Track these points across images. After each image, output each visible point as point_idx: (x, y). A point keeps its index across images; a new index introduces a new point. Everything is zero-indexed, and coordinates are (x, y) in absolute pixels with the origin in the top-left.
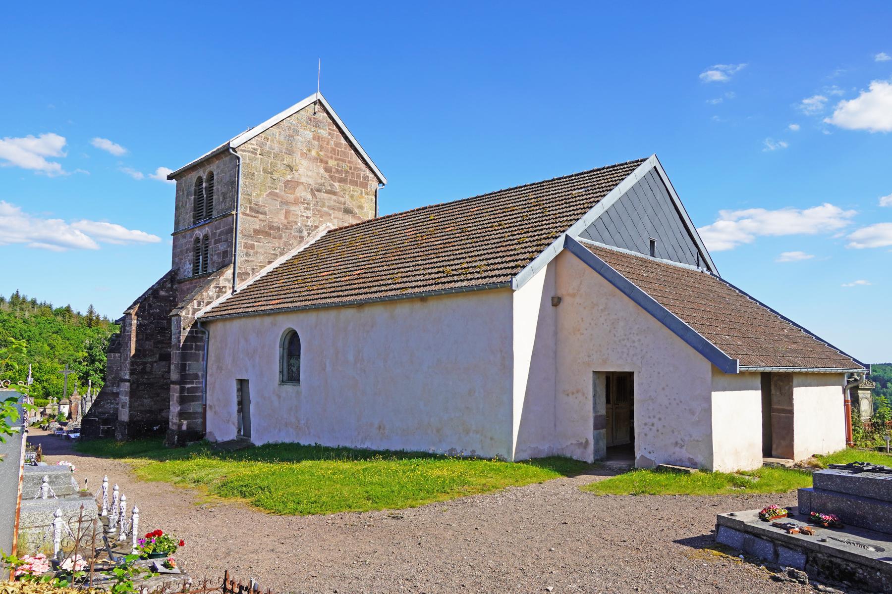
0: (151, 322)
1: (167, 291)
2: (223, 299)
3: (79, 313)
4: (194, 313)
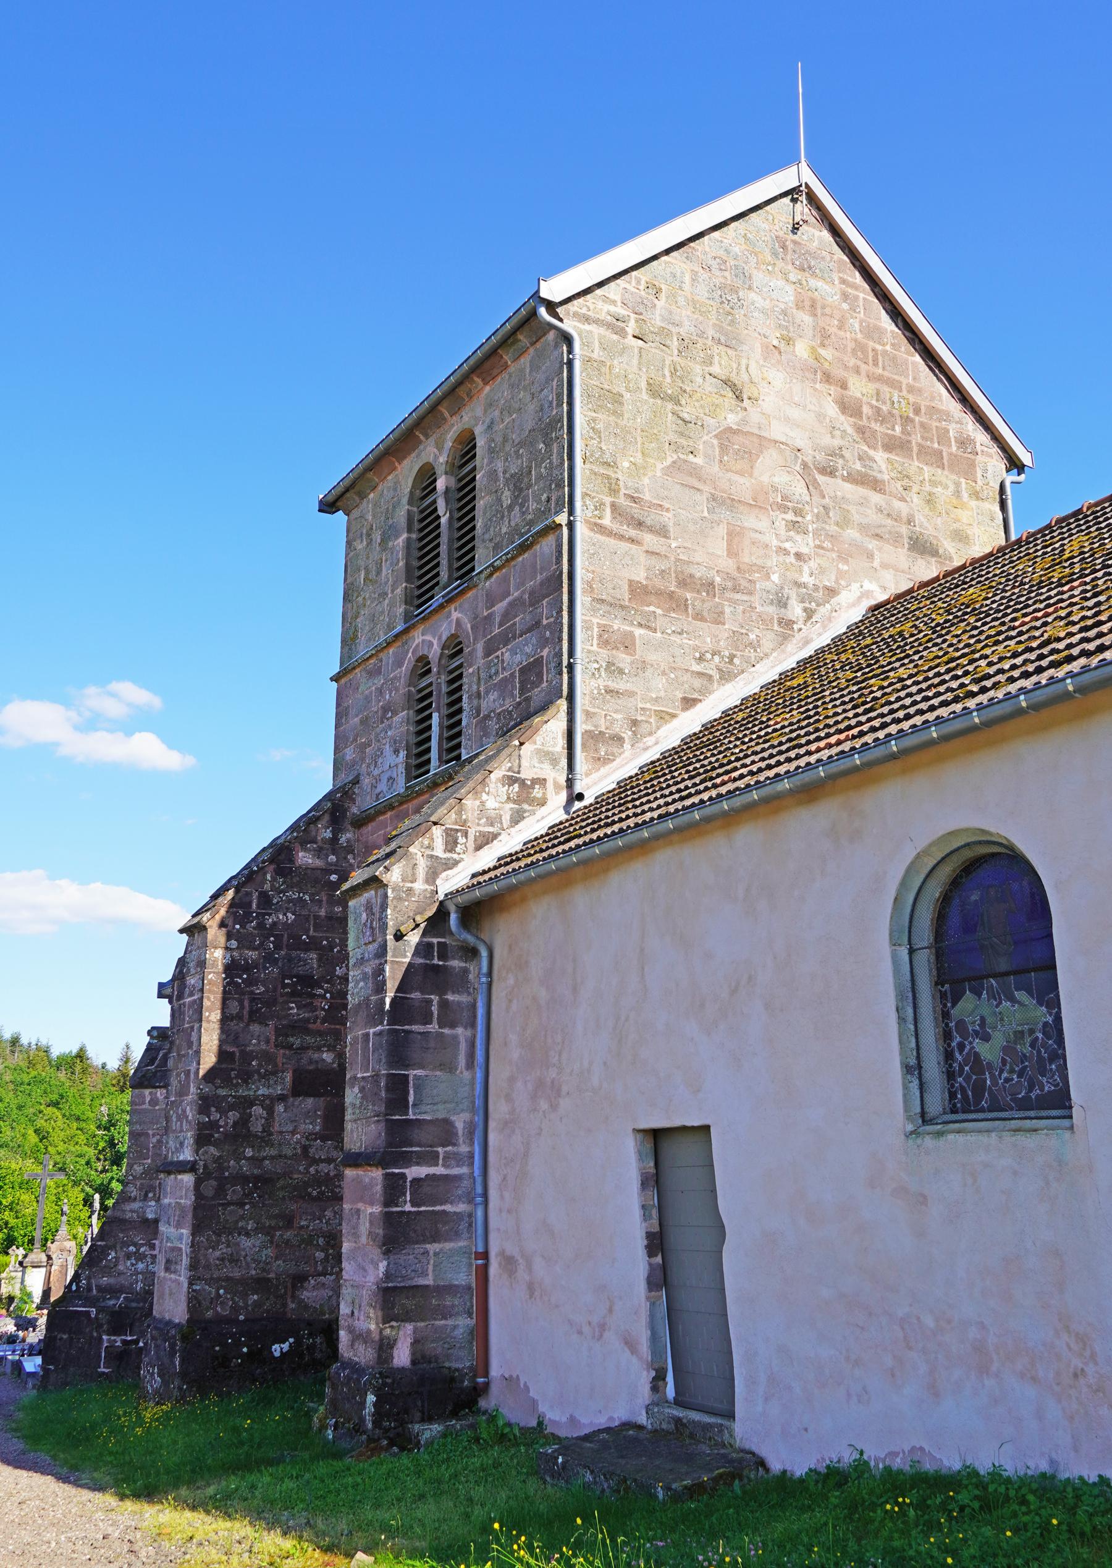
0: (269, 958)
1: (319, 853)
2: (536, 825)
3: (104, 1066)
4: (432, 877)
